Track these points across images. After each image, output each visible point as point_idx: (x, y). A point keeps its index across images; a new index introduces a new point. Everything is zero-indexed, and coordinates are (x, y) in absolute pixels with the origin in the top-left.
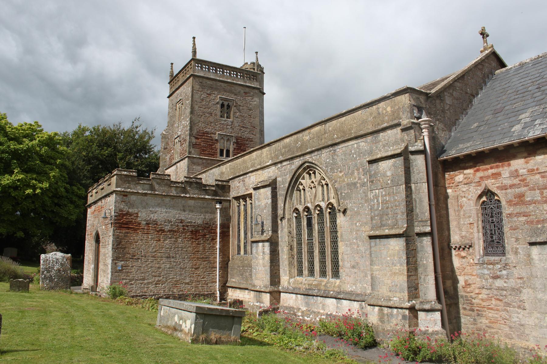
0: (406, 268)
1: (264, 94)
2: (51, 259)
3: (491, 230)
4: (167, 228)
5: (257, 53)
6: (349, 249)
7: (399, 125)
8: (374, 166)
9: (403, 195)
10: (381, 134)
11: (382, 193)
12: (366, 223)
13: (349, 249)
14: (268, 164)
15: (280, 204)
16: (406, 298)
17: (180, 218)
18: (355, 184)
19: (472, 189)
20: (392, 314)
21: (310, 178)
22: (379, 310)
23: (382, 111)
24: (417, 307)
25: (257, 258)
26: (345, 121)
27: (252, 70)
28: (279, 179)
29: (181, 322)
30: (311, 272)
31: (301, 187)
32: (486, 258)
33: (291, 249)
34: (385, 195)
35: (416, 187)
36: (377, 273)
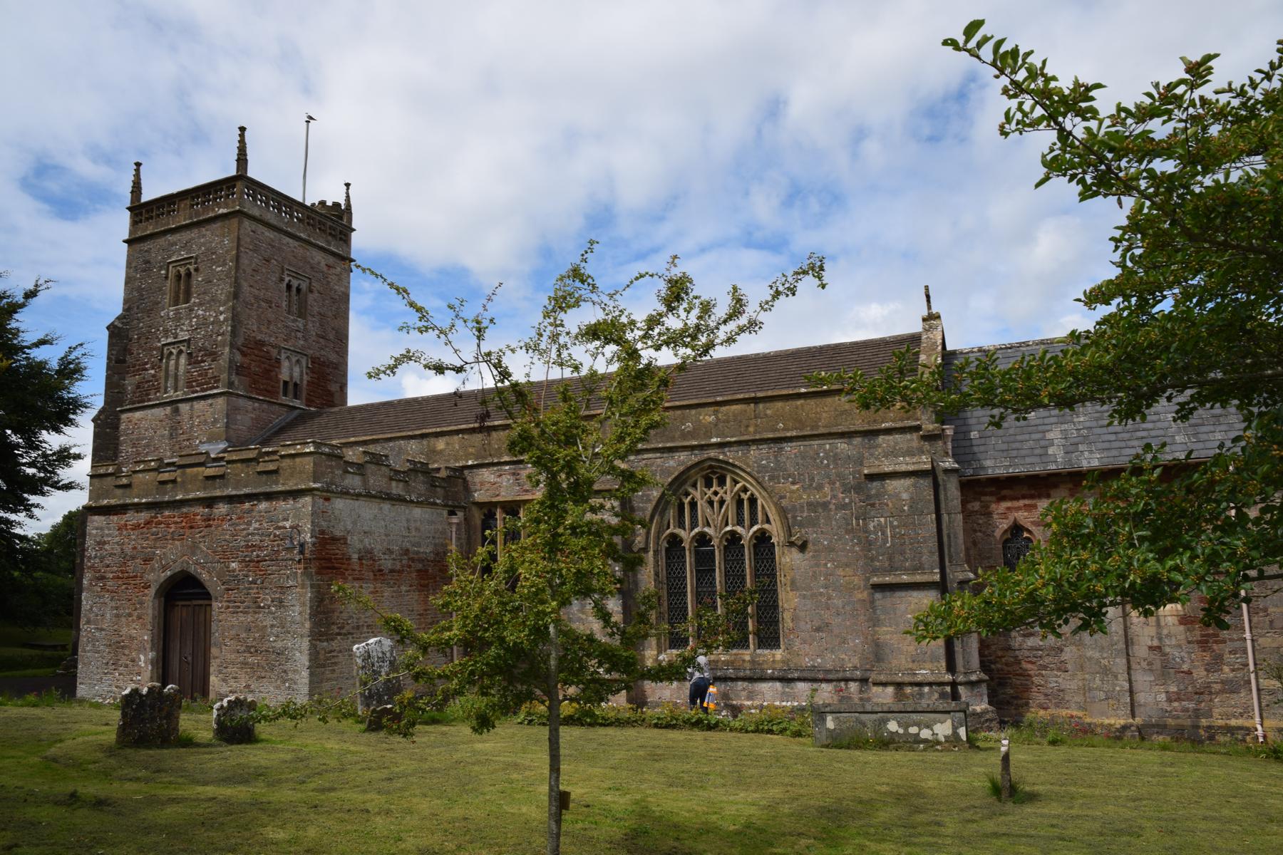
7: (918, 428)
13: (808, 602)
18: (825, 505)
29: (913, 730)
34: (898, 527)
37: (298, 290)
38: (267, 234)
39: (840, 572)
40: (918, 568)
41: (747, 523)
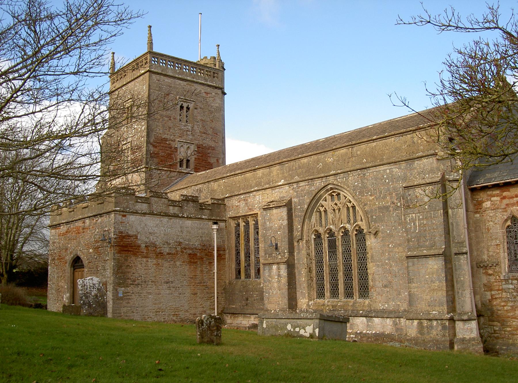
0: (445, 284)
1: (225, 94)
2: (88, 284)
3: (515, 251)
4: (166, 250)
5: (219, 46)
6: (380, 269)
8: (411, 192)
9: (441, 219)
10: (416, 162)
11: (419, 217)
12: (400, 245)
13: (380, 269)
14: (280, 184)
15: (297, 226)
16: (446, 311)
17: (178, 240)
18: (387, 208)
19: (499, 215)
20: (432, 326)
21: (332, 200)
22: (418, 323)
23: (417, 141)
24: (456, 318)
25: (270, 282)
26: (375, 146)
27: (212, 66)
28: (295, 200)
29: (297, 329)
30: (335, 293)
31: (322, 209)
32: (511, 275)
33: (310, 271)
34: (423, 219)
35: (452, 212)
36: (416, 290)
37: (188, 108)
38: (166, 80)
39: (396, 250)
40: (431, 247)
41: (352, 221)
